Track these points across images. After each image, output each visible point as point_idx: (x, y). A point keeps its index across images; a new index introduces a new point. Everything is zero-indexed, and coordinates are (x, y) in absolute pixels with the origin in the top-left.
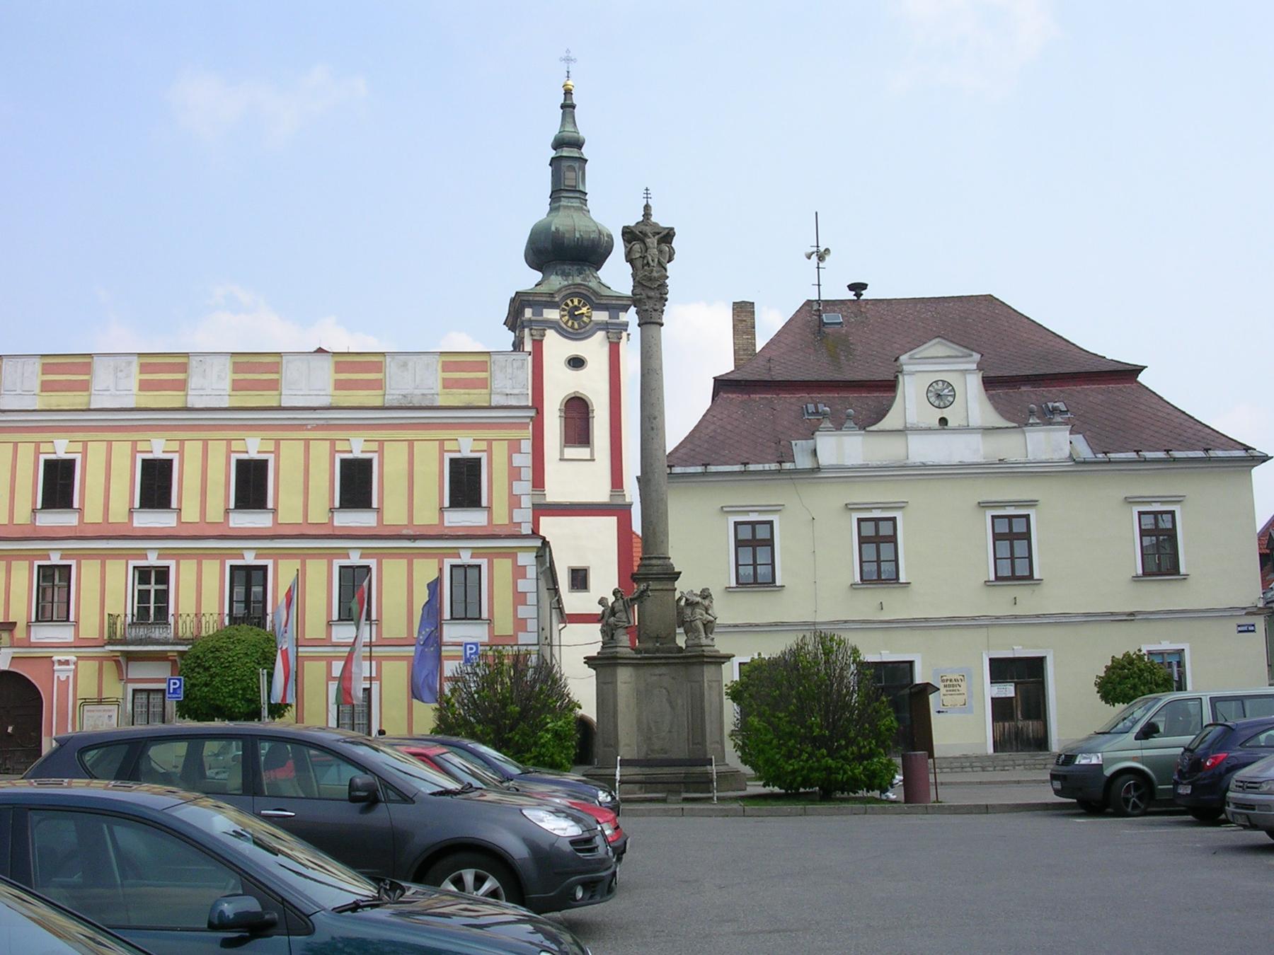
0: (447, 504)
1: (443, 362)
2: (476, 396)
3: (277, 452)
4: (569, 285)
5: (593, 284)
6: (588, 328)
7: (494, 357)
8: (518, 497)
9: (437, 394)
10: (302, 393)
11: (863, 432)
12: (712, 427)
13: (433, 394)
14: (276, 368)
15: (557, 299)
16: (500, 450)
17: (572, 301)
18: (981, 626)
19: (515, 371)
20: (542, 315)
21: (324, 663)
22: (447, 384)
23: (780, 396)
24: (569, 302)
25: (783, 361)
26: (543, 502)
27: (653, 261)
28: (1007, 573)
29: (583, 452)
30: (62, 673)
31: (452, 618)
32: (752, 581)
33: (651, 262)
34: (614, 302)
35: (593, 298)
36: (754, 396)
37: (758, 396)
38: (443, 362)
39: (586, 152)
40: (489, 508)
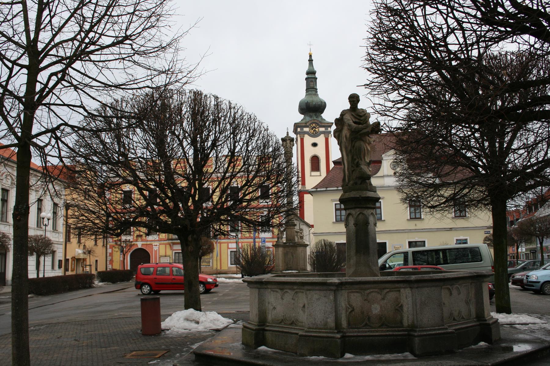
5: (320, 119)
18: (406, 232)
21: (226, 244)
28: (414, 217)
29: (317, 173)
30: (155, 248)
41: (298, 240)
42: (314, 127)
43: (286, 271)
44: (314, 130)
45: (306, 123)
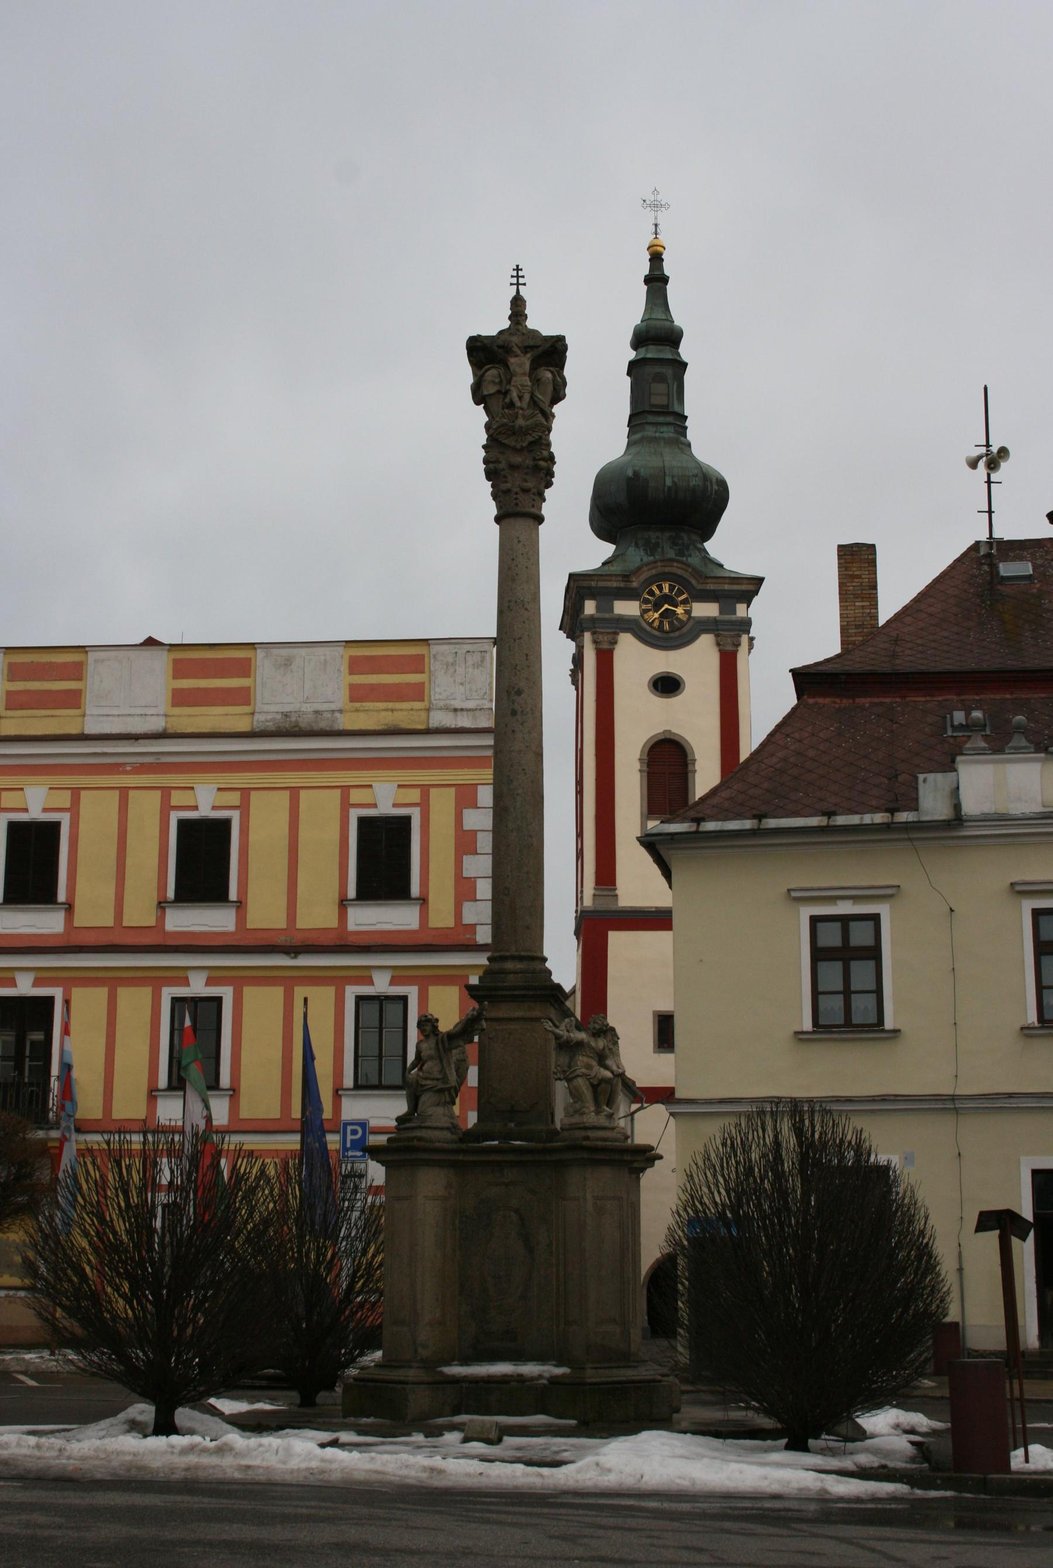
0: (352, 893)
1: (351, 657)
2: (404, 714)
3: (74, 810)
4: (655, 562)
5: (694, 560)
6: (684, 630)
7: (435, 649)
8: (471, 882)
9: (341, 711)
10: (116, 712)
11: (1042, 755)
12: (780, 754)
13: (333, 711)
14: (77, 671)
15: (635, 585)
16: (443, 803)
17: (660, 588)
19: (470, 670)
20: (611, 609)
22: (357, 694)
23: (908, 699)
24: (654, 588)
25: (919, 641)
26: (613, 907)
27: (520, 398)
31: (357, 1086)
32: (842, 1022)
33: (516, 399)
34: (727, 587)
35: (693, 582)
36: (863, 700)
37: (868, 700)
38: (351, 657)
39: (686, 351)
40: (423, 900)
41: (575, 1109)
42: (667, 599)
43: (465, 1361)
44: (666, 614)
45: (626, 577)
